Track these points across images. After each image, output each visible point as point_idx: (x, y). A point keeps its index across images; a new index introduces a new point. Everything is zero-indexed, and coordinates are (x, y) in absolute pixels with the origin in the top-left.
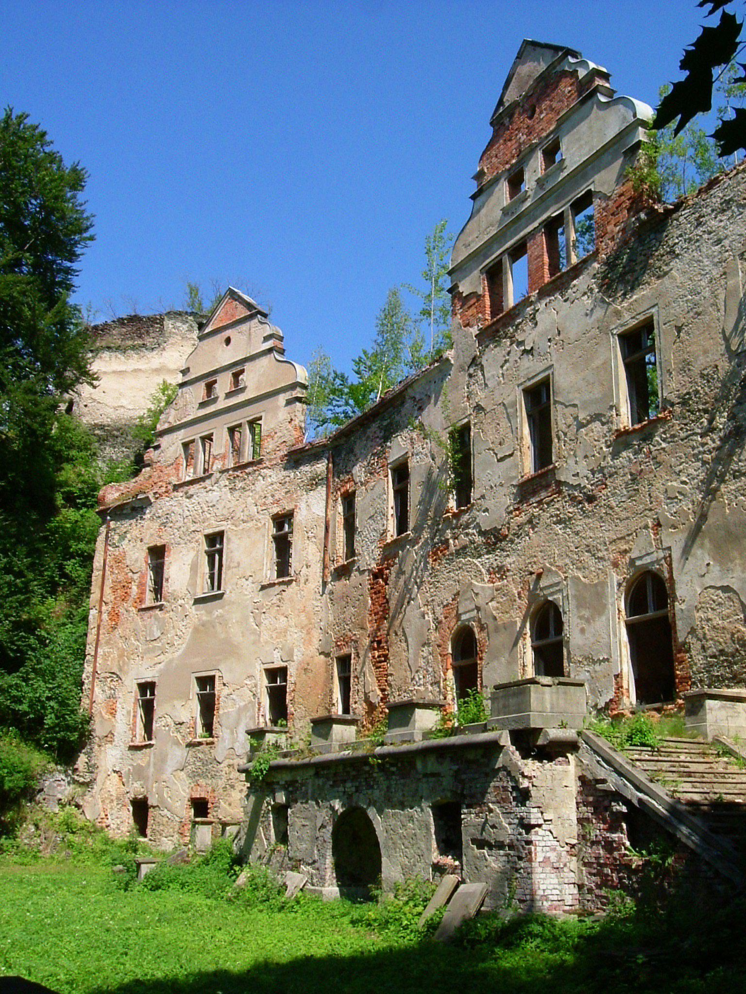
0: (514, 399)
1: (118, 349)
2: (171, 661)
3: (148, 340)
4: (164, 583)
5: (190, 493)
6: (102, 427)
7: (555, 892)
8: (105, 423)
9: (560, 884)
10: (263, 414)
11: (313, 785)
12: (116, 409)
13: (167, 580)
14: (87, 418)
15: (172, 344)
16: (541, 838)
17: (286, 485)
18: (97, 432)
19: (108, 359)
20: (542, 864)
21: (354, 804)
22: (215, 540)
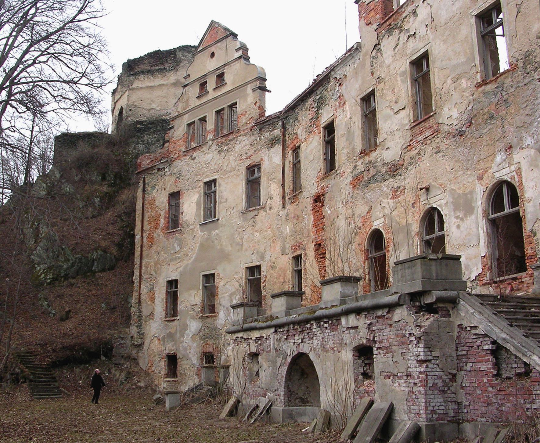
0: (404, 70)
1: (149, 72)
2: (187, 265)
3: (167, 66)
4: (181, 216)
5: (194, 156)
6: (141, 123)
7: (441, 408)
8: (143, 120)
9: (445, 402)
10: (238, 100)
11: (274, 339)
12: (149, 110)
13: (182, 213)
14: (132, 118)
15: (183, 66)
16: (431, 370)
17: (255, 146)
18: (138, 126)
19: (142, 79)
20: (432, 388)
21: (301, 351)
22: (210, 184)
